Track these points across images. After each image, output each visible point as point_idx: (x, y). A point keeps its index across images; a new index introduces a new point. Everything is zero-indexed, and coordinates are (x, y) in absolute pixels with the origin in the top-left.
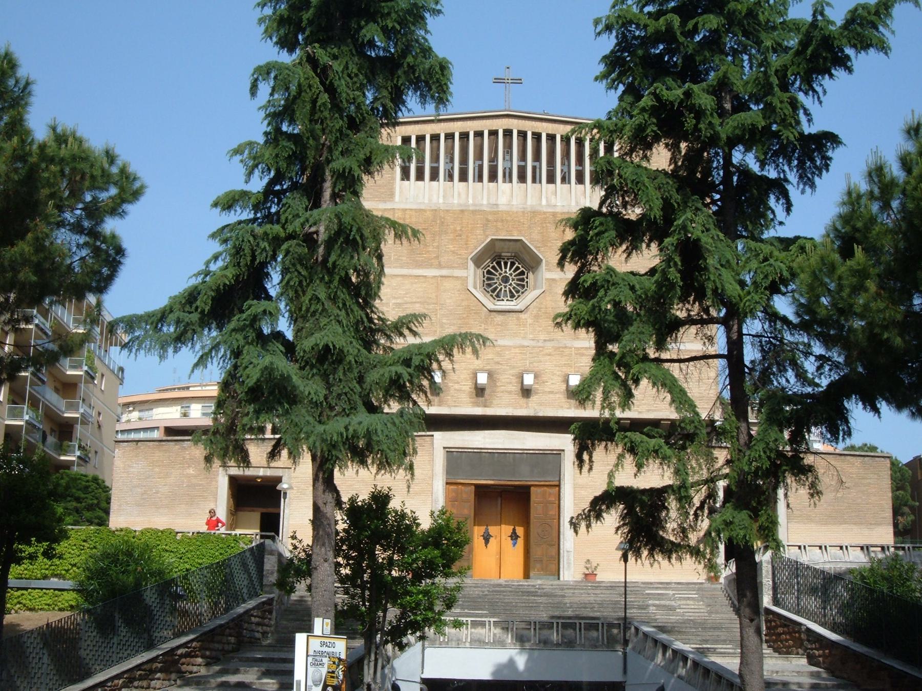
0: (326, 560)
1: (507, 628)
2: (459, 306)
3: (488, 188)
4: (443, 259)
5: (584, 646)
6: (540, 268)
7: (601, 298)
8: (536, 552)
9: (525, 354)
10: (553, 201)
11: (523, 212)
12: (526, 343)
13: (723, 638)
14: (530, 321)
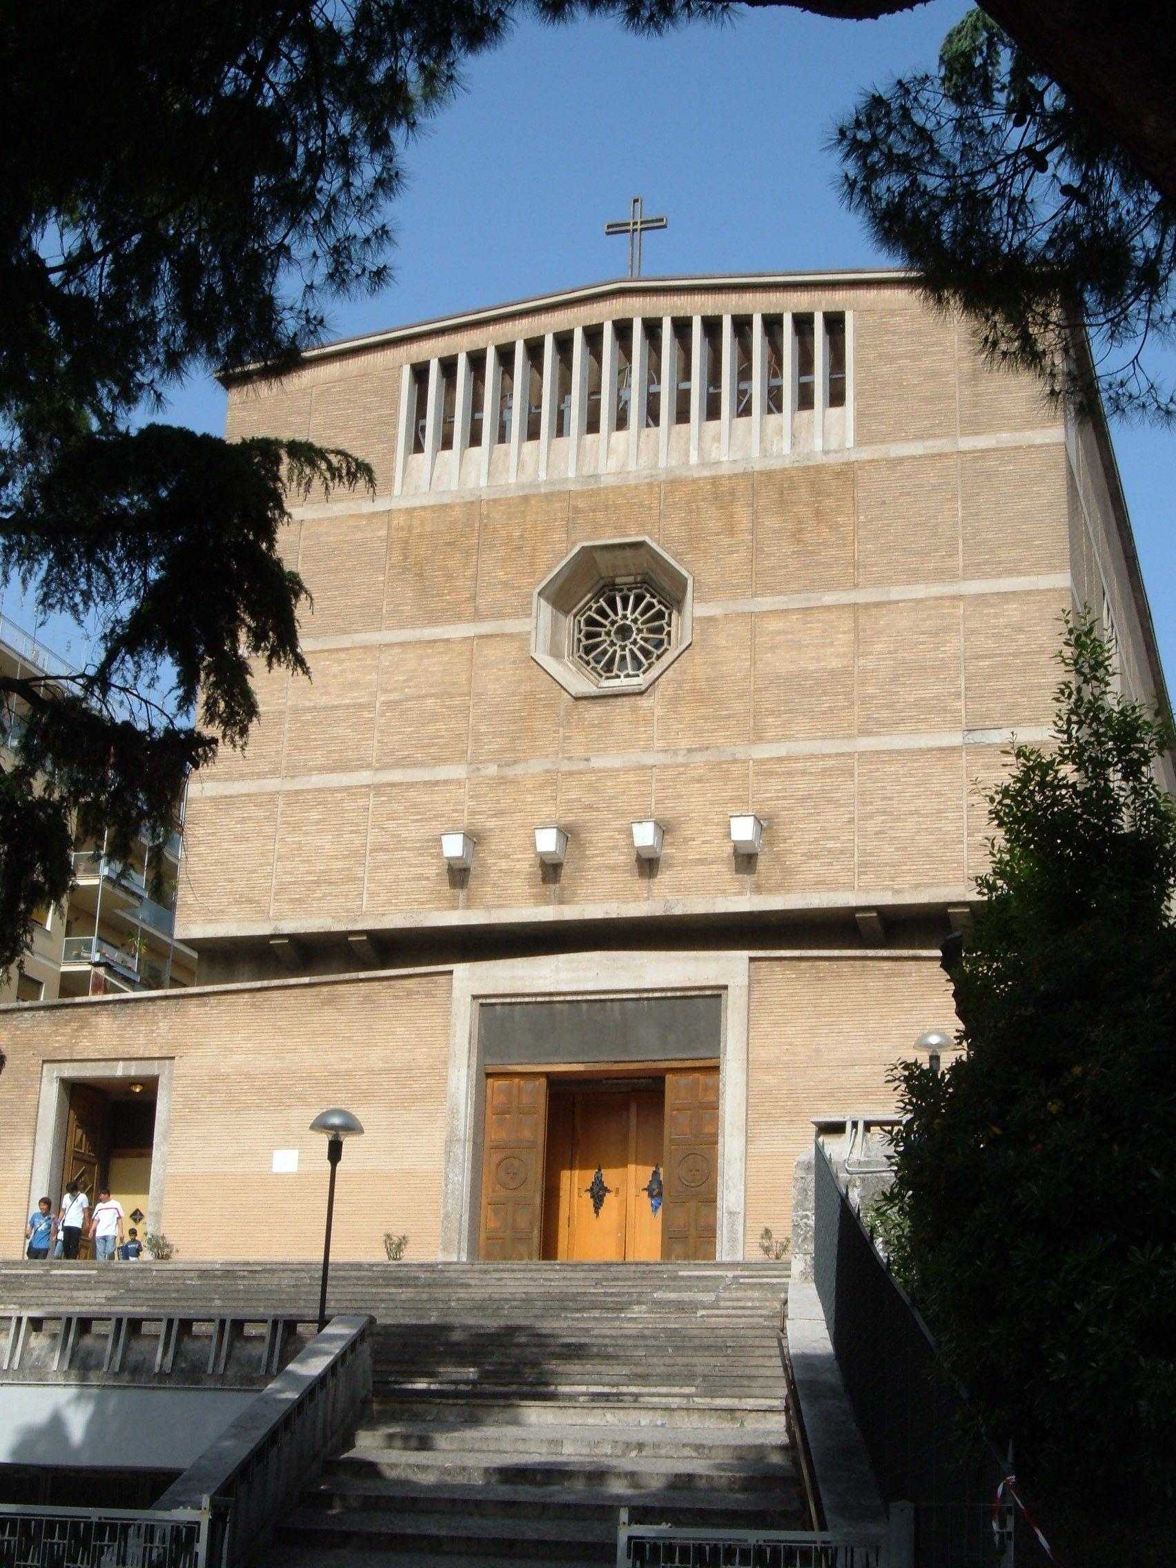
2: (513, 694)
9: (648, 783)
10: (714, 456)
11: (650, 485)
12: (649, 759)
14: (659, 712)
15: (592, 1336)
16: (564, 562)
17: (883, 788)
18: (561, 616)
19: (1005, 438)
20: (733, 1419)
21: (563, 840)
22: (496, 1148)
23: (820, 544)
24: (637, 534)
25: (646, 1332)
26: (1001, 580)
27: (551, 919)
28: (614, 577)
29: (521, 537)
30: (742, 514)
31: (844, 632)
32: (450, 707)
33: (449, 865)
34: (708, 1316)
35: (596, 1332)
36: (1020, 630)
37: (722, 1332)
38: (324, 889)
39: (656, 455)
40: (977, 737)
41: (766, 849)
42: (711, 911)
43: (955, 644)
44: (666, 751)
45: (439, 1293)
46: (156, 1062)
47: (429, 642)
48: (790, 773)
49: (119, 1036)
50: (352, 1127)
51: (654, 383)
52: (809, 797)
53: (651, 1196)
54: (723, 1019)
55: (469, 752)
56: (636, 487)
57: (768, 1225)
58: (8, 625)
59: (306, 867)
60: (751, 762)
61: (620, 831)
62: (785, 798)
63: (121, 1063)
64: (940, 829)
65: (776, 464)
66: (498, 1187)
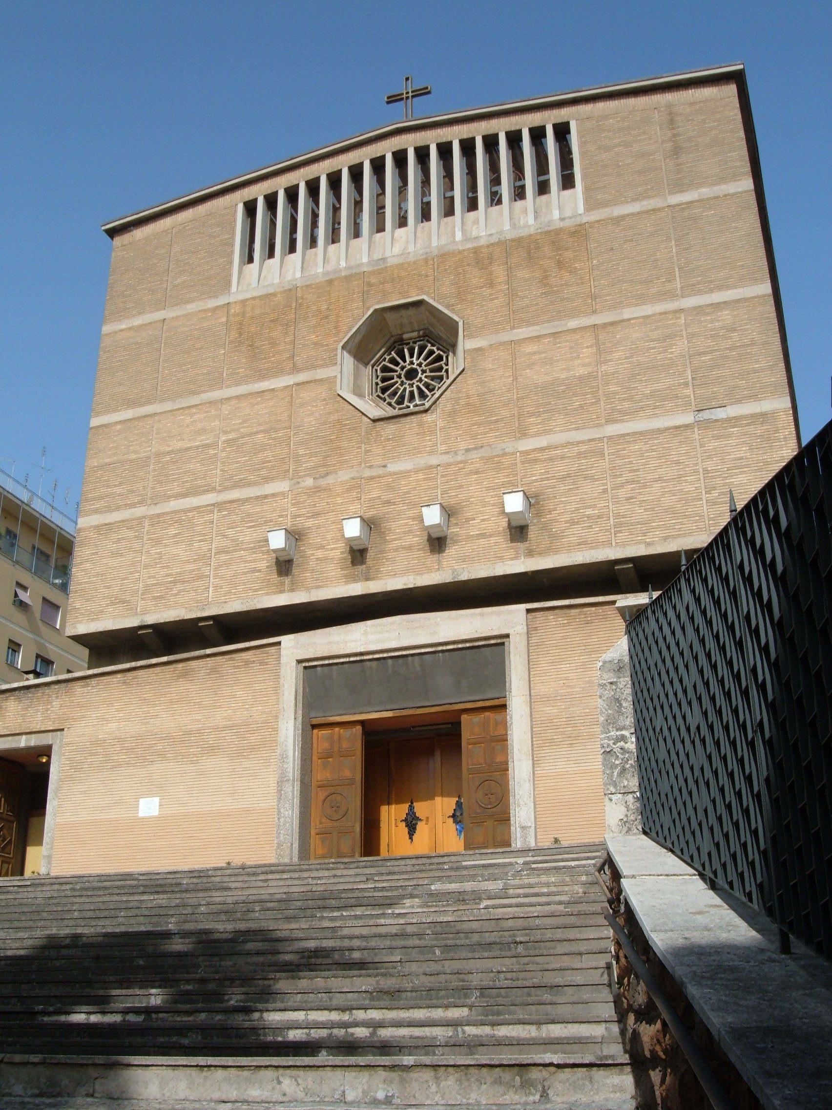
2: (325, 423)
10: (475, 233)
11: (426, 260)
12: (434, 460)
15: (343, 938)
17: (630, 463)
18: (361, 366)
19: (706, 192)
20: (527, 1085)
21: (367, 529)
23: (562, 285)
25: (410, 929)
26: (713, 295)
27: (359, 593)
29: (328, 309)
30: (499, 272)
31: (587, 347)
33: (277, 558)
34: (494, 907)
35: (346, 932)
36: (734, 330)
37: (511, 923)
38: (179, 586)
39: (430, 239)
40: (706, 415)
41: (535, 521)
42: (492, 575)
43: (680, 347)
45: (192, 898)
46: (50, 734)
47: (258, 393)
48: (551, 459)
49: (22, 715)
51: (426, 196)
52: (569, 475)
53: (456, 822)
54: (507, 663)
55: (291, 471)
56: (415, 263)
57: (556, 836)
58: (64, 518)
59: (166, 571)
60: (518, 454)
61: (413, 519)
62: (548, 479)
63: (24, 737)
65: (524, 232)
66: (324, 820)
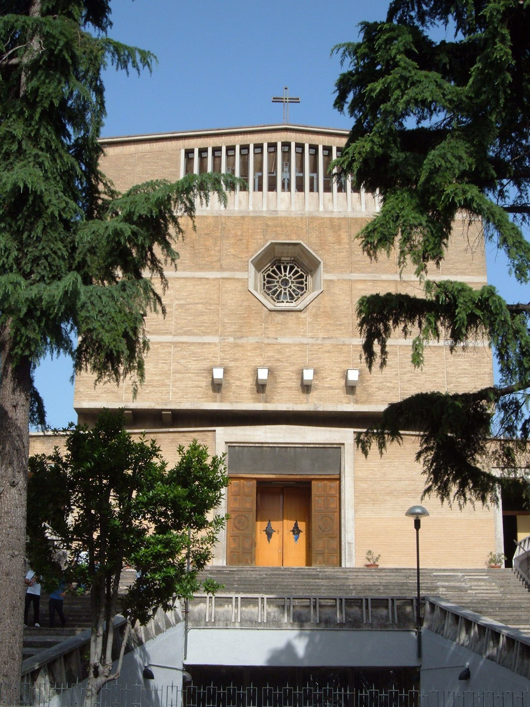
0: (13, 485)
1: (283, 606)
3: (268, 197)
4: (225, 263)
5: (371, 625)
6: (318, 271)
7: (397, 100)
8: (318, 545)
9: (305, 351)
10: (330, 208)
11: (302, 218)
12: (305, 341)
13: (524, 618)
14: (309, 320)
16: (263, 249)
22: (234, 511)
24: (296, 239)
27: (261, 409)
28: (281, 257)
32: (209, 309)
44: (312, 338)
50: (425, 513)
53: (294, 534)
56: (295, 218)
64: (435, 381)
66: (235, 529)
